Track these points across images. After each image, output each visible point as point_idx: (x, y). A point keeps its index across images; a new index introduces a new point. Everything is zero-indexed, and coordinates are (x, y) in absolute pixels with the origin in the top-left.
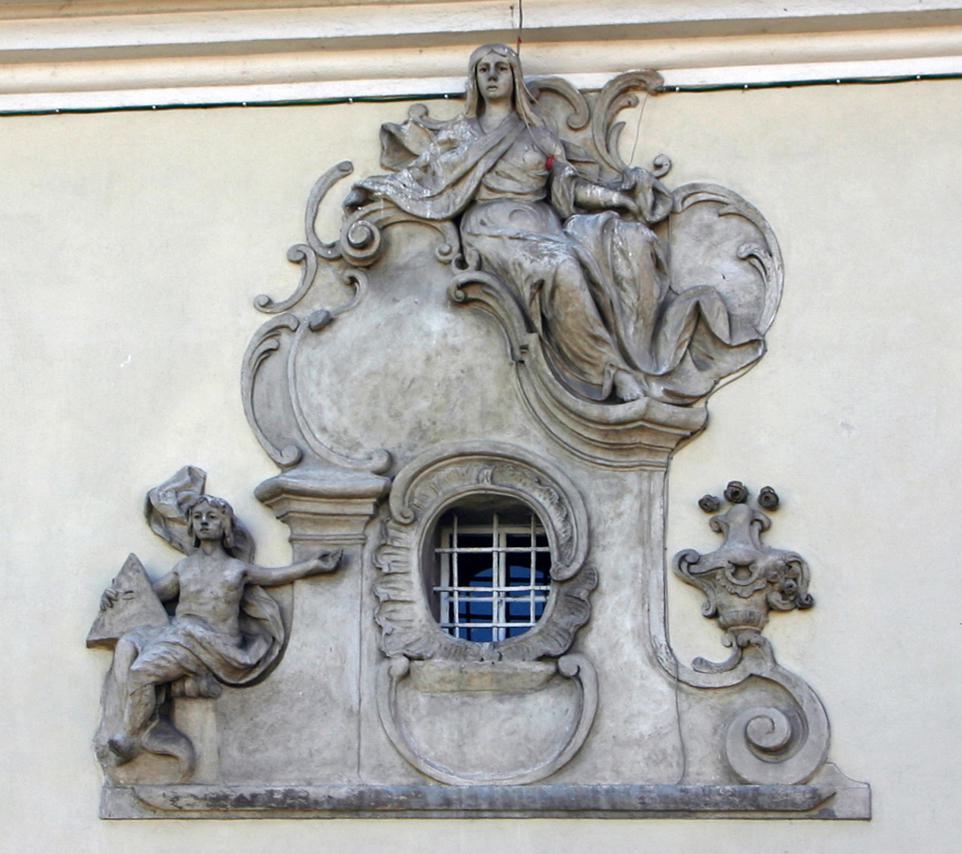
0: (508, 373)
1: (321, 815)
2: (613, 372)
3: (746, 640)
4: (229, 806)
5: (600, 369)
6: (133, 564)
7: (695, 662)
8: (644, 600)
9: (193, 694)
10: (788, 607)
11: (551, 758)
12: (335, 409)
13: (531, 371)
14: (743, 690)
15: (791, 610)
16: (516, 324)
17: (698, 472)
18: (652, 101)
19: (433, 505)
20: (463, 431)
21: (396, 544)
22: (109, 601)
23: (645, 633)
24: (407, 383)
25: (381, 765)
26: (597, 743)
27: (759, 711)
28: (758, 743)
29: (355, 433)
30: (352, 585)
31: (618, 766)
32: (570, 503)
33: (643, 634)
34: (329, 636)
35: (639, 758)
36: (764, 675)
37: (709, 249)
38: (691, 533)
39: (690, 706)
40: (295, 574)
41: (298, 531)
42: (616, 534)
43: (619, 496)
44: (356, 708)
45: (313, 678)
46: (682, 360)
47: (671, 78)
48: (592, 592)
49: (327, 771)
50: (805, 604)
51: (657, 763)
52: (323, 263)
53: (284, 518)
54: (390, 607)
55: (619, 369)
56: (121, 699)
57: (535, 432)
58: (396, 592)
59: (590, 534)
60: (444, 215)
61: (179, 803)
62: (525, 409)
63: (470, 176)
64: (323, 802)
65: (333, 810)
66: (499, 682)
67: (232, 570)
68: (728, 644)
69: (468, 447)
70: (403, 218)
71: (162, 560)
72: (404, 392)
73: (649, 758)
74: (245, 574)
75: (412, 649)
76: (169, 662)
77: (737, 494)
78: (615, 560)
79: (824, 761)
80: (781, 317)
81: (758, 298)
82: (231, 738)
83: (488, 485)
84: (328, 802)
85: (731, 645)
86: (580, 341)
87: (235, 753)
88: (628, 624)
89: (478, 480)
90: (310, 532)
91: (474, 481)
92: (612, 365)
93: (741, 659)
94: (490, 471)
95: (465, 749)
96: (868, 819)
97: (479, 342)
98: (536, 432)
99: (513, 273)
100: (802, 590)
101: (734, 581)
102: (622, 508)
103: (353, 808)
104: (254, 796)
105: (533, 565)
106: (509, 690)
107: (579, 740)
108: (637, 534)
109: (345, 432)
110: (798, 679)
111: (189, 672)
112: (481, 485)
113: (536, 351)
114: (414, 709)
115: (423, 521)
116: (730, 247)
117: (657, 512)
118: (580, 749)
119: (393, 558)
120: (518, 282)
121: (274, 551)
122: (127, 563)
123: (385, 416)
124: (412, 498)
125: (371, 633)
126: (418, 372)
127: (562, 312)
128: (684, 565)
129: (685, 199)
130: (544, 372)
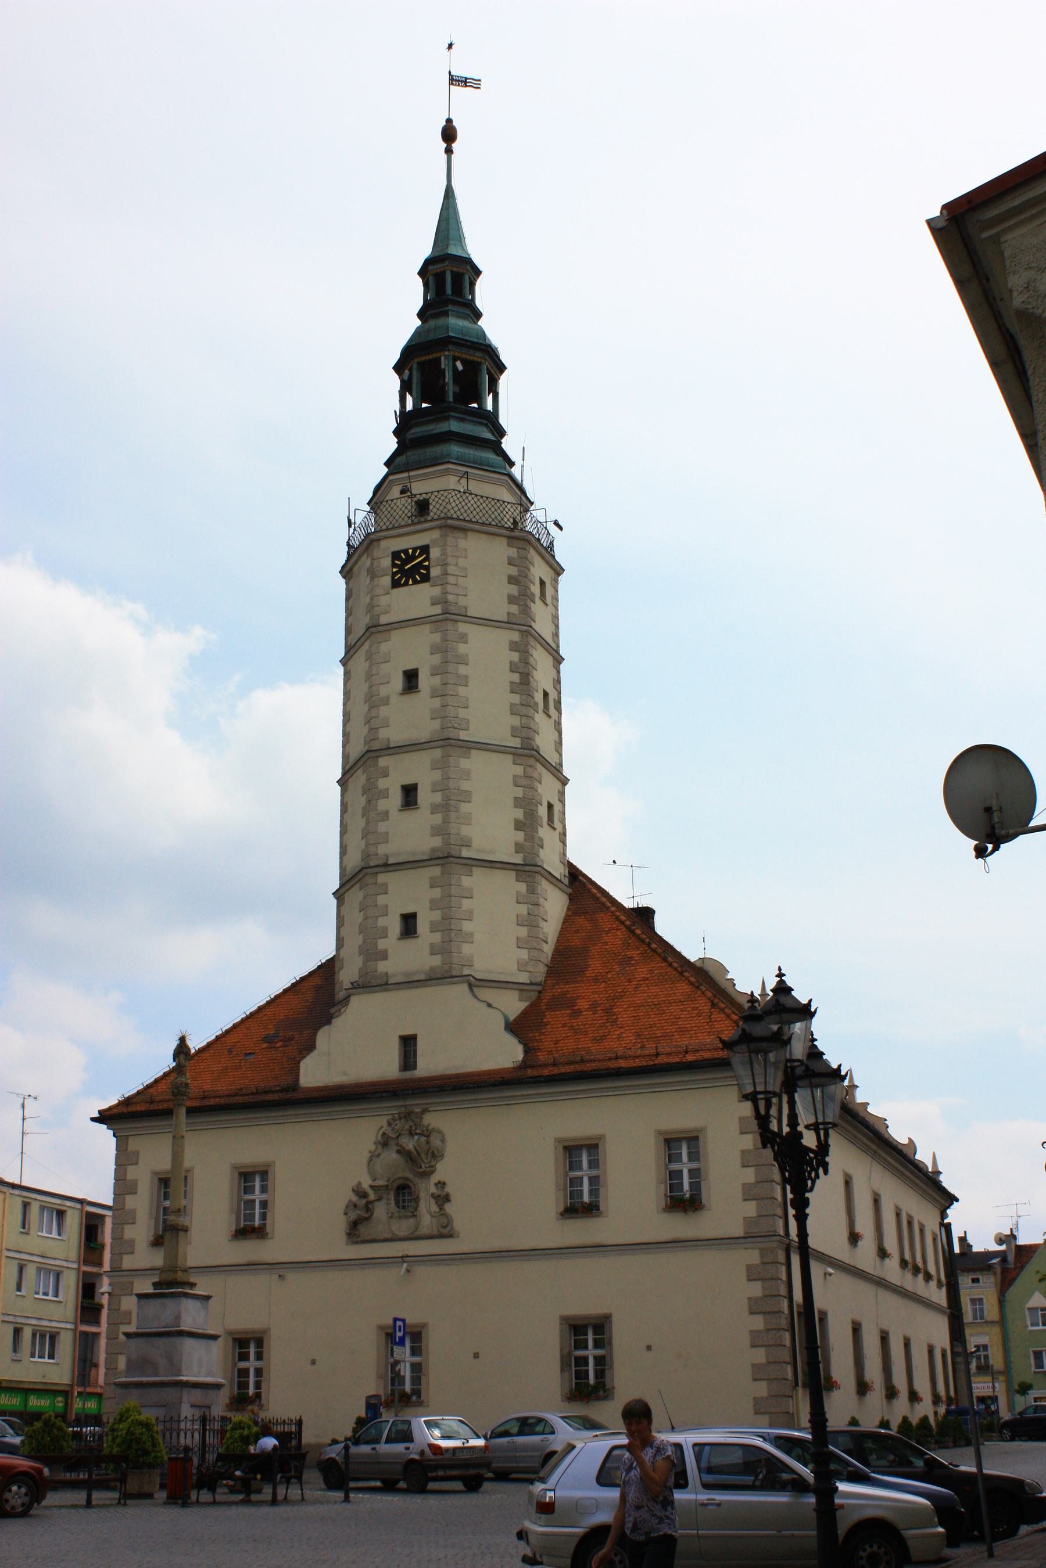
3: (441, 1207)
6: (350, 1201)
17: (434, 1179)
19: (395, 1185)
23: (427, 1207)
30: (384, 1201)
31: (424, 1230)
34: (380, 1211)
38: (433, 1189)
62: (750, 1245)
67: (364, 1201)
71: (354, 1198)
78: (422, 1194)
106: (406, 1217)
108: (426, 1189)
121: (372, 1196)
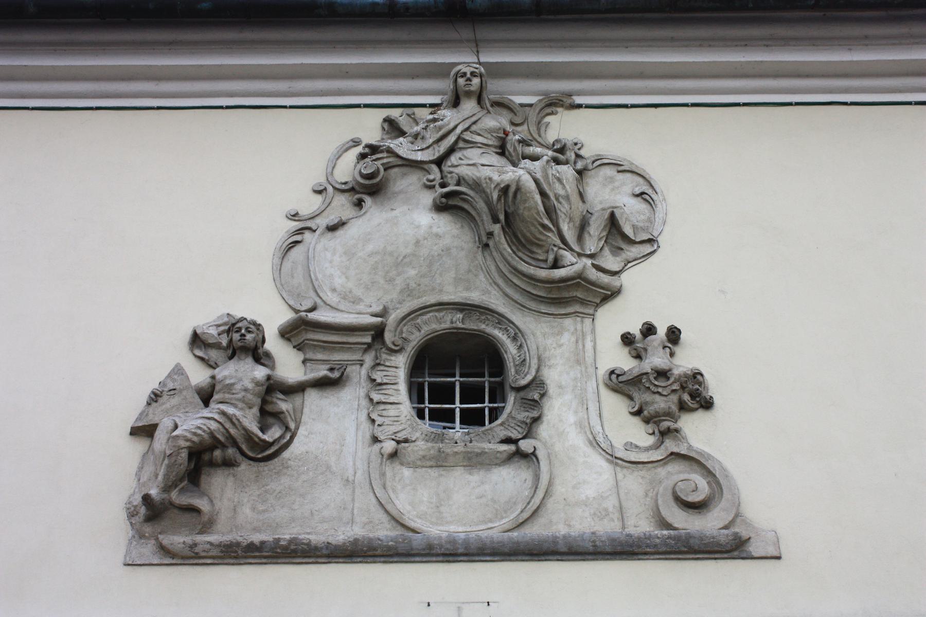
0: (477, 253)
1: (320, 560)
2: (555, 249)
3: (663, 427)
4: (240, 552)
5: (545, 249)
6: (178, 370)
7: (626, 444)
8: (583, 402)
9: (219, 461)
10: (696, 406)
11: (514, 515)
12: (343, 277)
13: (493, 250)
14: (665, 464)
15: (697, 409)
16: (485, 218)
17: (615, 320)
18: (567, 112)
19: (416, 339)
20: (441, 291)
21: (387, 364)
22: (155, 397)
24: (401, 258)
25: (371, 522)
26: (550, 504)
27: (682, 476)
28: (685, 498)
29: (358, 292)
32: (523, 336)
33: (584, 426)
35: (587, 514)
36: (682, 452)
37: (613, 190)
39: (625, 476)
40: (307, 381)
41: (310, 355)
42: (558, 358)
43: (560, 333)
44: (351, 478)
45: (316, 457)
46: (601, 249)
47: (578, 100)
48: (543, 396)
49: (326, 526)
50: (708, 405)
51: (601, 519)
52: (338, 194)
53: (299, 347)
54: (382, 407)
55: (560, 248)
56: (156, 465)
57: (495, 292)
58: (387, 397)
59: (539, 359)
60: (431, 158)
61: (197, 550)
63: (452, 134)
64: (322, 548)
65: (328, 556)
66: (470, 459)
68: (651, 432)
69: (445, 298)
70: (400, 163)
72: (397, 265)
73: (595, 514)
74: (269, 378)
75: (399, 435)
76: (204, 431)
77: (649, 330)
78: (557, 375)
79: (737, 515)
80: (667, 229)
81: (649, 218)
82: (245, 500)
83: (460, 325)
84: (327, 548)
85: (653, 433)
86: (532, 228)
87: (247, 510)
88: (572, 419)
89: (452, 322)
90: (320, 356)
91: (448, 323)
92: (555, 245)
93: (662, 442)
94: (461, 316)
95: (442, 509)
96: (779, 558)
97: (455, 232)
98: (495, 292)
99: (484, 185)
100: (704, 394)
101: (656, 383)
102: (562, 341)
103: (348, 553)
104: (263, 543)
105: (487, 390)
107: (537, 501)
108: (571, 366)
109: (350, 292)
110: (709, 455)
111: (199, 476)
112: (454, 325)
113: (499, 236)
114: (400, 480)
115: (409, 349)
116: (628, 189)
117: (589, 345)
118: (538, 508)
119: (385, 373)
120: (488, 191)
122: (173, 369)
123: (382, 281)
124: (402, 332)
125: (366, 426)
126: (409, 251)
127: (522, 208)
128: (614, 376)
129: (593, 162)
130: (505, 249)
